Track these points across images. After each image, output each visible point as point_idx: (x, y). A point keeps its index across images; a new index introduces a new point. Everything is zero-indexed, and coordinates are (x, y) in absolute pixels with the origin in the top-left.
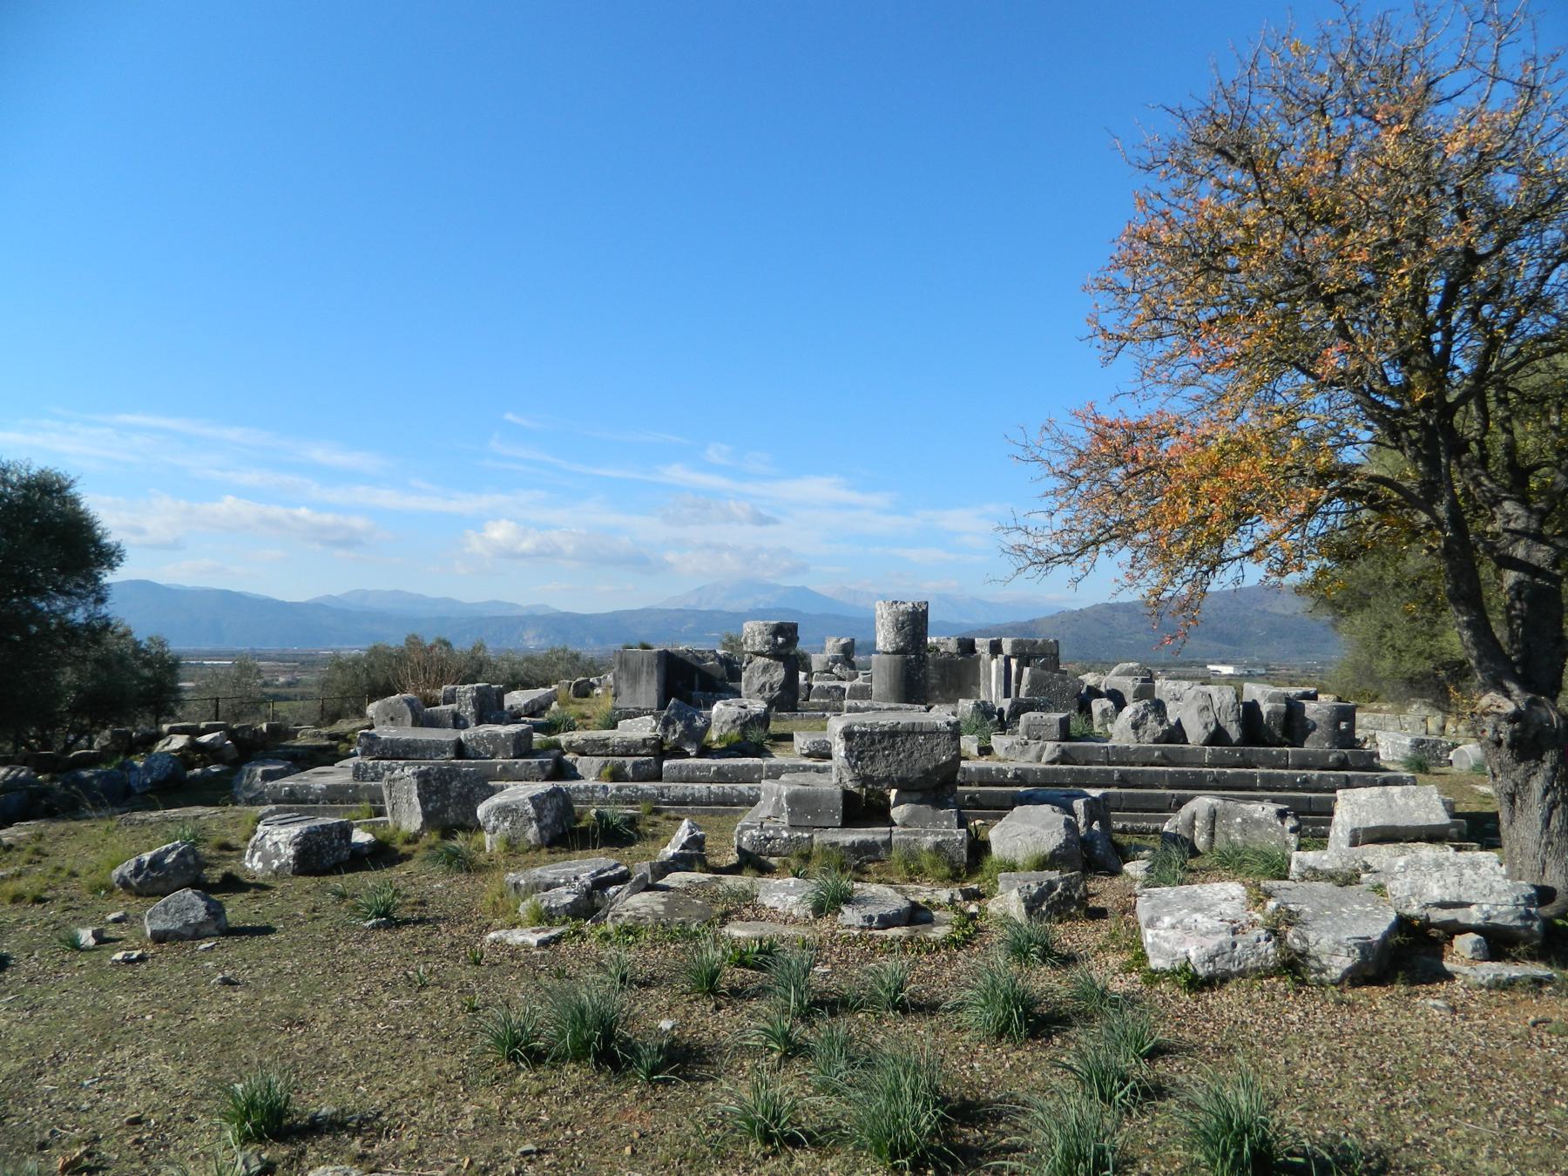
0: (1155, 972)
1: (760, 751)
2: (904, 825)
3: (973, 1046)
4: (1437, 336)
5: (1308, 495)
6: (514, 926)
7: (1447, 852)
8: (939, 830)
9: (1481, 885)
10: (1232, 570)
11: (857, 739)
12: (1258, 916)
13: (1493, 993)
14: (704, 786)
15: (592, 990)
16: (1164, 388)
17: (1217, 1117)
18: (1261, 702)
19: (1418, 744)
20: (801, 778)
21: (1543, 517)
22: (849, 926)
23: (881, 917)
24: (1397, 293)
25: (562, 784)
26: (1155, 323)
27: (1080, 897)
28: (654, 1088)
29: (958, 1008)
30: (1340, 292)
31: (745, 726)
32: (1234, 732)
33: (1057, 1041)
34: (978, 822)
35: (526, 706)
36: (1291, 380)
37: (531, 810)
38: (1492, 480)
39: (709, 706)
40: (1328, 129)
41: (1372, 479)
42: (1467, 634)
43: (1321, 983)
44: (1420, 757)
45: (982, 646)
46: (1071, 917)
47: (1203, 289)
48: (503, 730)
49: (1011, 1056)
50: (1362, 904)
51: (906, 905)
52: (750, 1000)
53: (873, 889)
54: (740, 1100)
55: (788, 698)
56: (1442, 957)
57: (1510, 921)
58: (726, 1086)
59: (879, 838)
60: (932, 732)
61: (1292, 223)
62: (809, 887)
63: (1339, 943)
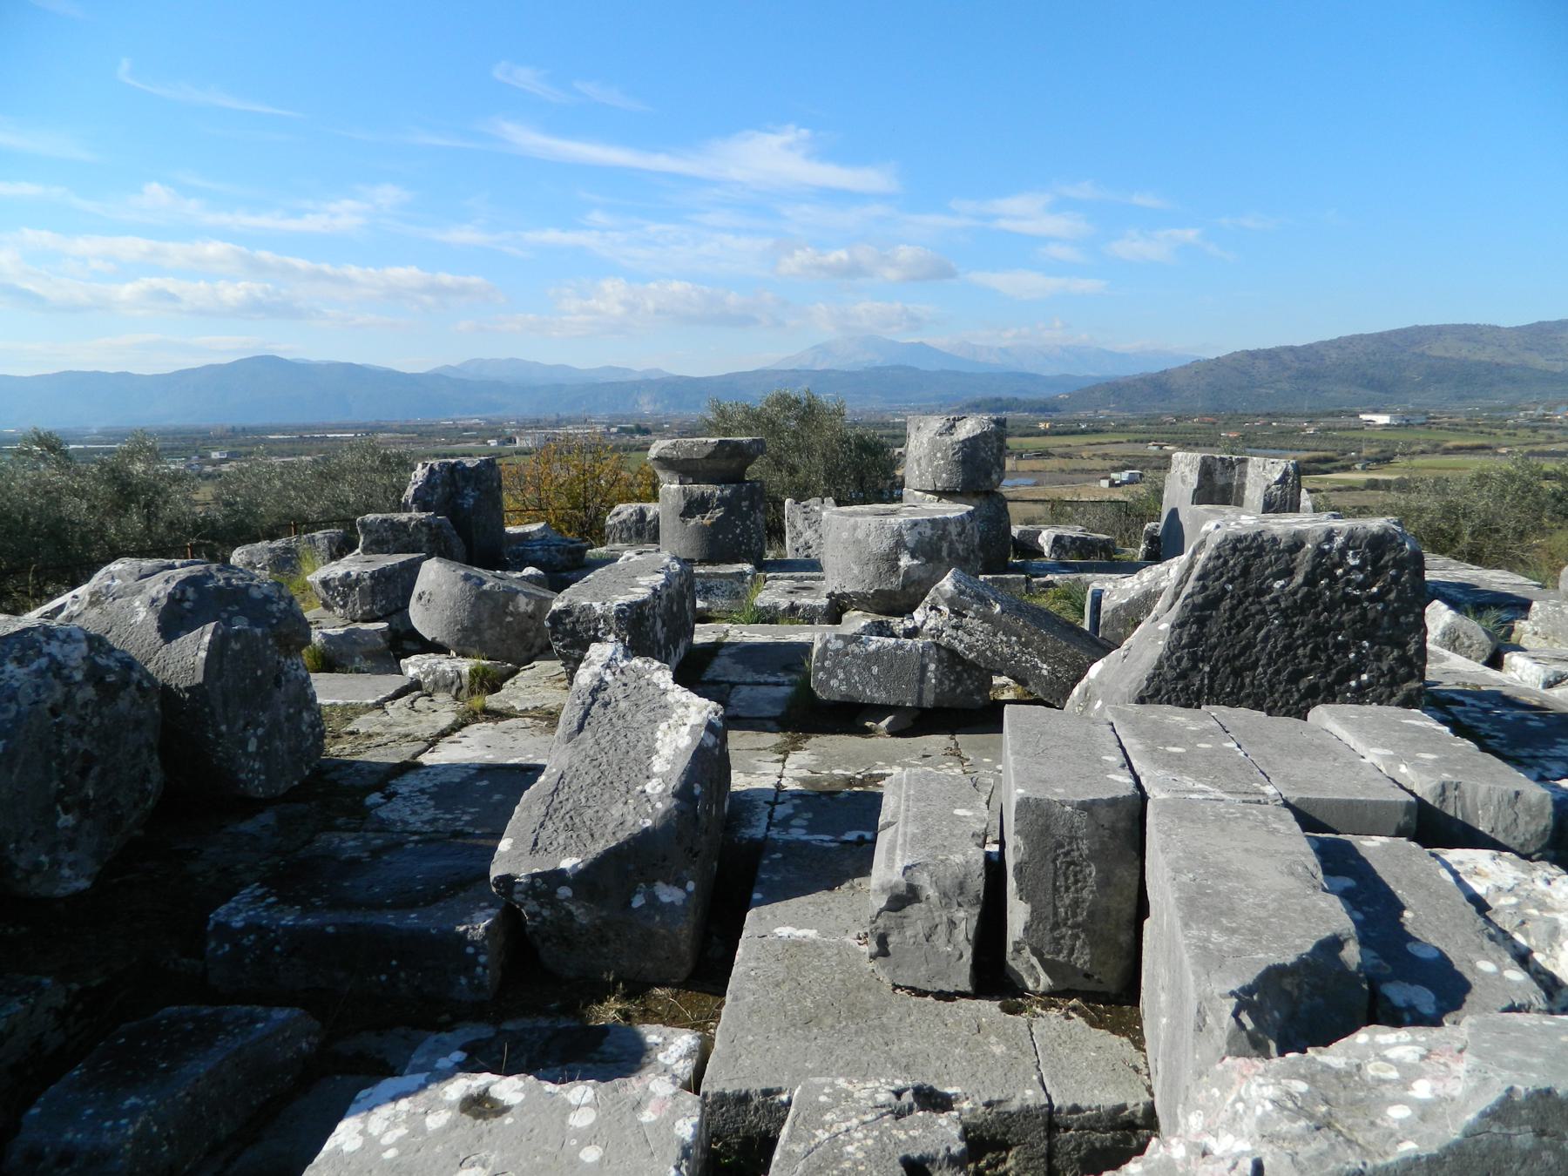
54: (924, 622)
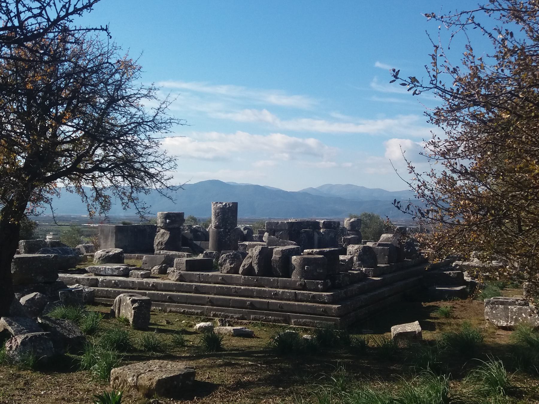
25: (322, 249)
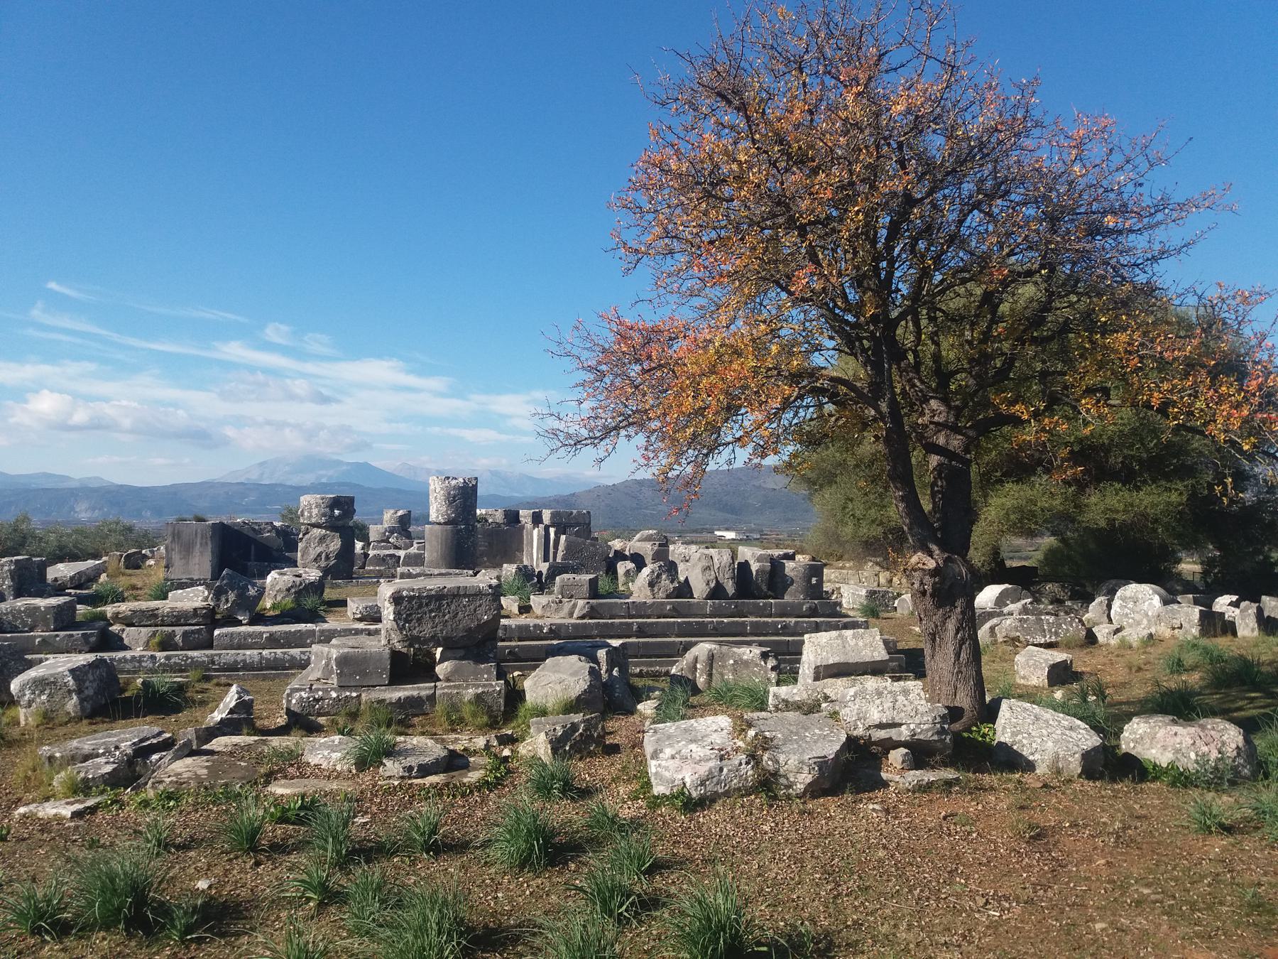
0: (658, 797)
1: (314, 617)
2: (448, 680)
3: (499, 878)
4: (884, 264)
5: (783, 392)
6: (47, 799)
7: (886, 683)
8: (483, 682)
9: (909, 708)
10: (726, 453)
11: (405, 603)
12: (740, 744)
13: (917, 795)
14: (256, 652)
15: (128, 856)
16: (675, 297)
17: (700, 920)
18: (751, 562)
19: (871, 594)
20: (351, 641)
21: (958, 412)
22: (390, 777)
23: (420, 766)
24: (853, 227)
25: (106, 655)
26: (667, 240)
27: (599, 736)
28: (187, 947)
29: (486, 844)
30: (810, 223)
31: (298, 593)
32: (730, 587)
33: (573, 866)
34: (516, 674)
35: (72, 578)
36: (775, 296)
37: (71, 683)
38: (923, 382)
39: (263, 575)
40: (804, 84)
41: (832, 379)
42: (902, 506)
43: (789, 797)
44: (873, 605)
45: (525, 515)
46: (591, 754)
47: (706, 213)
48: (41, 603)
49: (534, 882)
50: (821, 729)
51: (444, 753)
52: (289, 853)
53: (415, 740)
55: (344, 567)
56: (880, 769)
57: (929, 736)
58: (261, 939)
59: (423, 693)
60: (476, 595)
61: (776, 161)
62: (352, 743)
63: (802, 762)
